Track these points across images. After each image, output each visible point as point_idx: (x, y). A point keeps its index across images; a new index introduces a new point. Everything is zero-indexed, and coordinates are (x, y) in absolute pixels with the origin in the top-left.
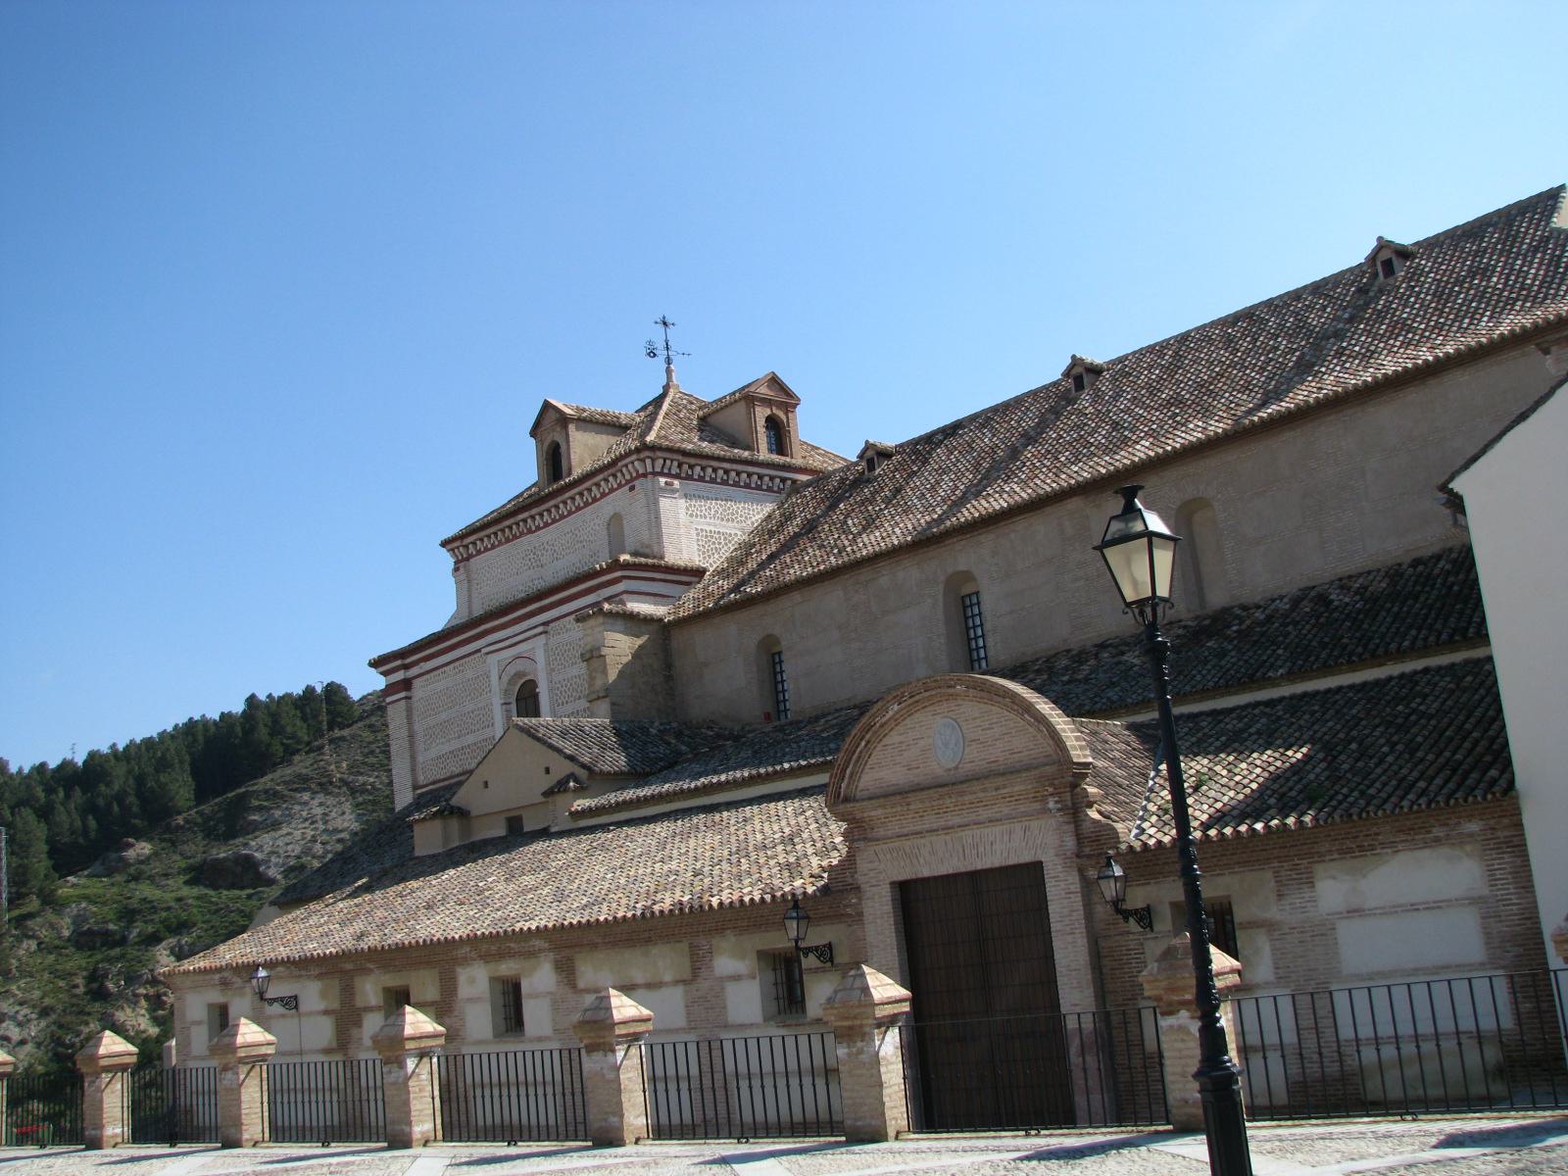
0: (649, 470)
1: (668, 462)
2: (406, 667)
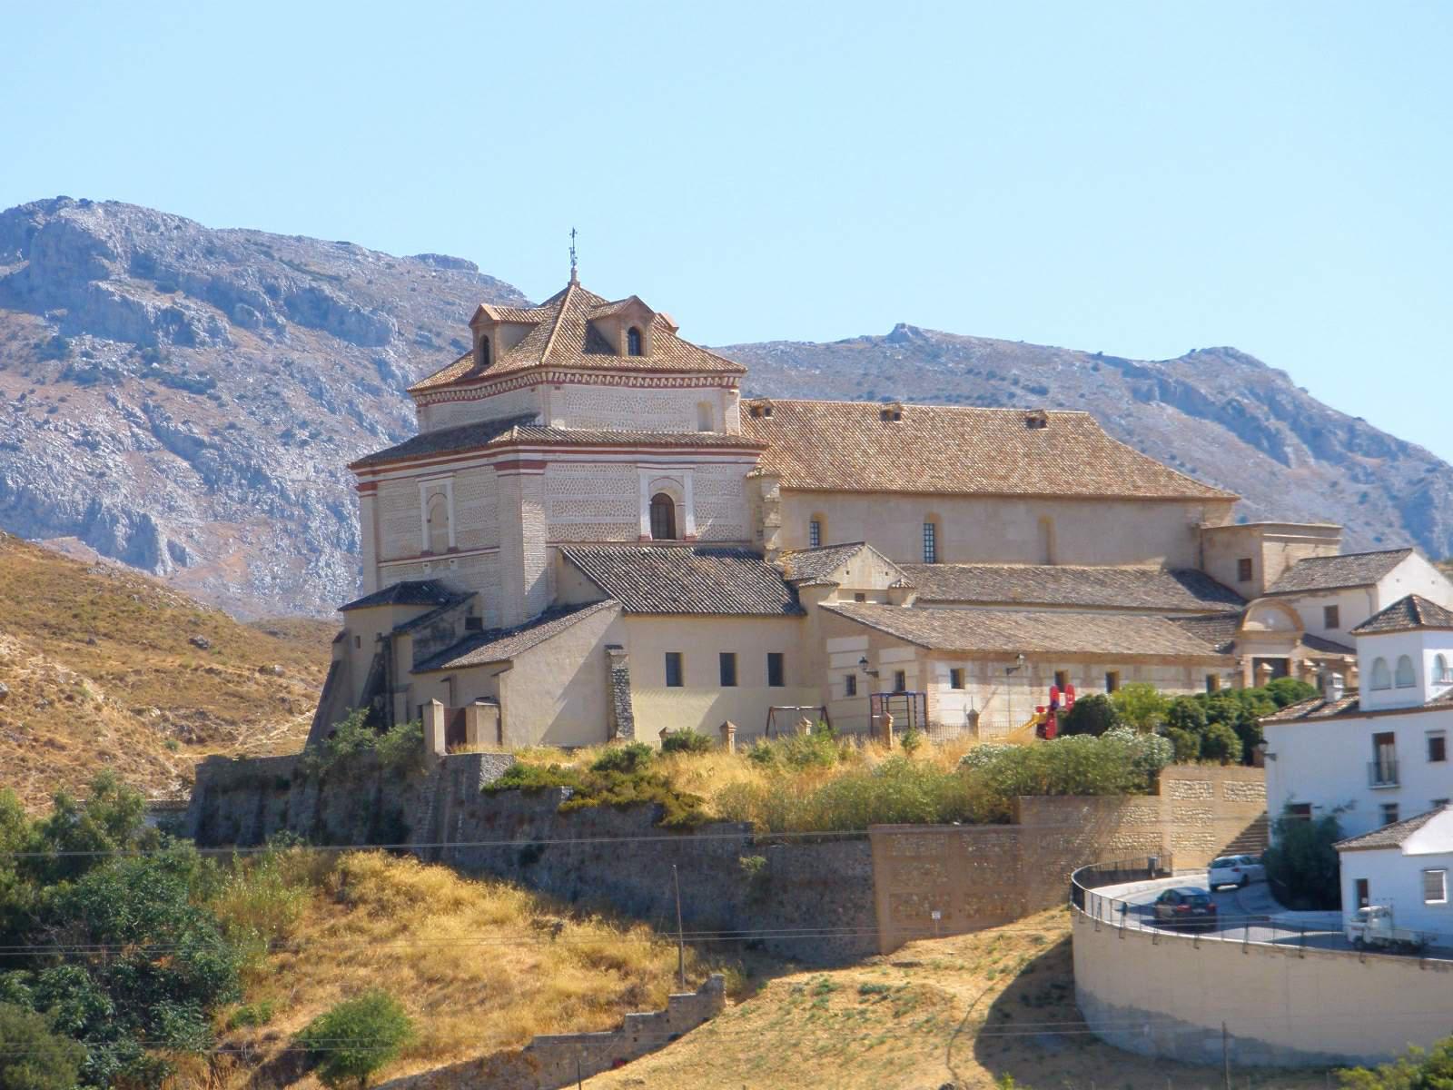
0: (545, 379)
1: (557, 375)
2: (374, 473)
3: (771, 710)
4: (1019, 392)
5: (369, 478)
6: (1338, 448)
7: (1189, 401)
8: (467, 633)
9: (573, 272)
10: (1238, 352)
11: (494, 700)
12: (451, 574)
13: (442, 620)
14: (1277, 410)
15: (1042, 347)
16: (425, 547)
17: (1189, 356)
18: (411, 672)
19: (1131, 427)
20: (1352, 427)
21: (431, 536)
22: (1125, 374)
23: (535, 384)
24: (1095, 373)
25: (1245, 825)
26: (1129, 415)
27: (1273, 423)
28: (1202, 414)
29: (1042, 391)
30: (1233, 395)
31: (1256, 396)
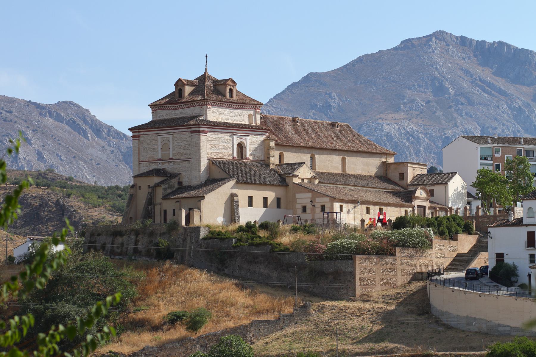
2: (139, 132)
3: (285, 216)
4: (3, 112)
5: (137, 134)
6: (105, 136)
7: (59, 118)
8: (178, 186)
9: (206, 69)
10: (74, 103)
11: (200, 209)
12: (170, 167)
13: (171, 182)
14: (85, 121)
15: (11, 98)
16: (160, 157)
17: (58, 103)
18: (162, 199)
19: (39, 125)
20: (110, 129)
21: (162, 154)
22: (37, 108)
23: (202, 105)
24: (28, 107)
25: (452, 259)
26: (39, 121)
27: (84, 126)
28: (62, 122)
29: (11, 112)
30: (71, 117)
31: (80, 118)
